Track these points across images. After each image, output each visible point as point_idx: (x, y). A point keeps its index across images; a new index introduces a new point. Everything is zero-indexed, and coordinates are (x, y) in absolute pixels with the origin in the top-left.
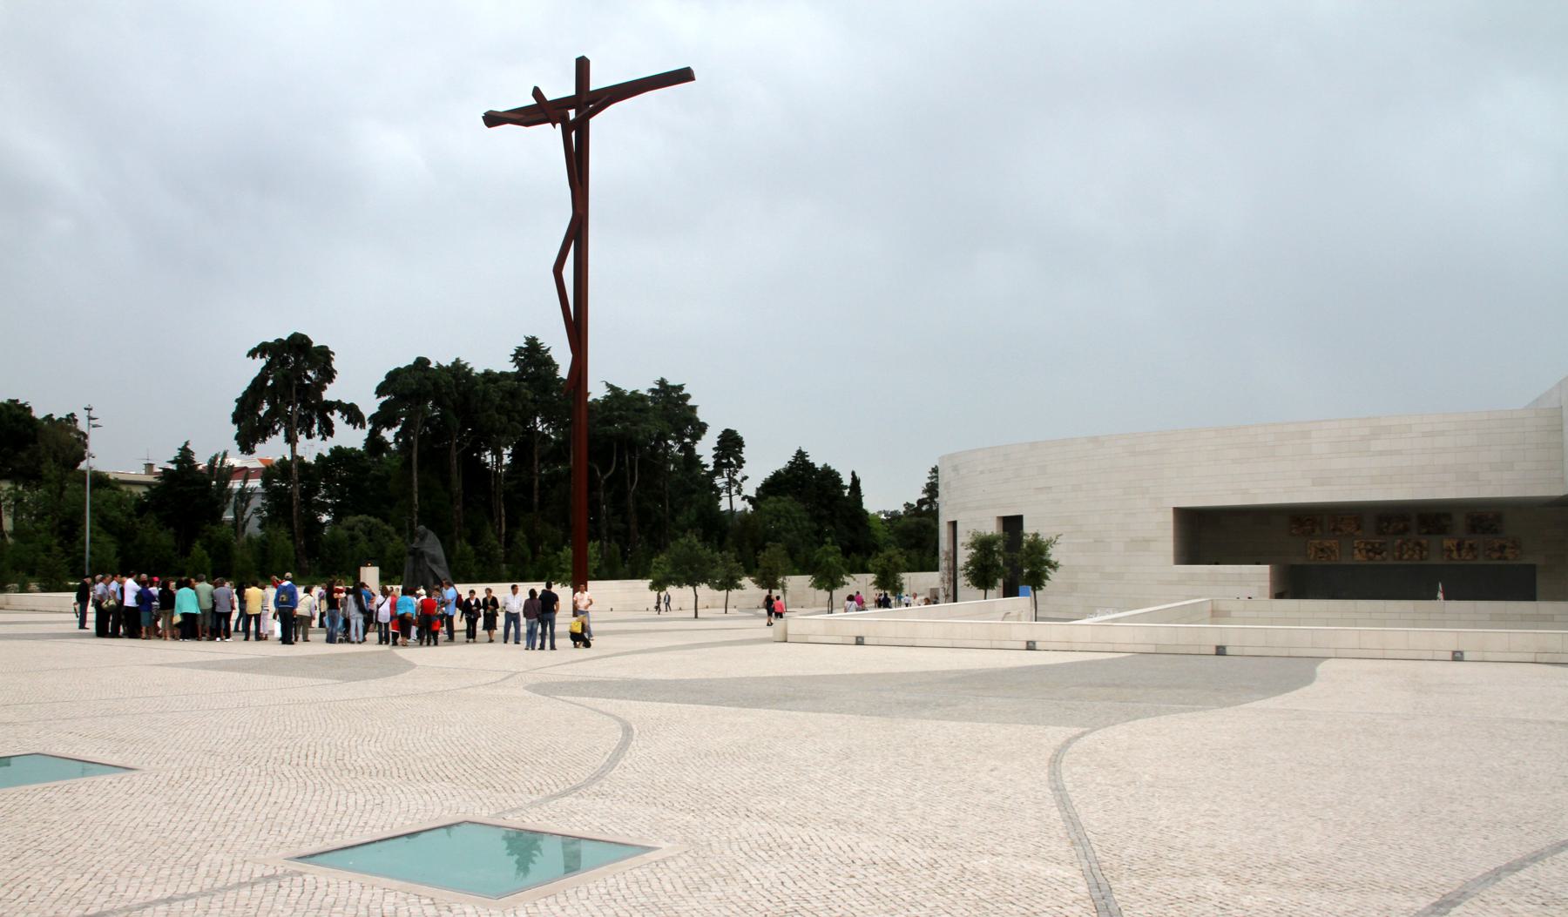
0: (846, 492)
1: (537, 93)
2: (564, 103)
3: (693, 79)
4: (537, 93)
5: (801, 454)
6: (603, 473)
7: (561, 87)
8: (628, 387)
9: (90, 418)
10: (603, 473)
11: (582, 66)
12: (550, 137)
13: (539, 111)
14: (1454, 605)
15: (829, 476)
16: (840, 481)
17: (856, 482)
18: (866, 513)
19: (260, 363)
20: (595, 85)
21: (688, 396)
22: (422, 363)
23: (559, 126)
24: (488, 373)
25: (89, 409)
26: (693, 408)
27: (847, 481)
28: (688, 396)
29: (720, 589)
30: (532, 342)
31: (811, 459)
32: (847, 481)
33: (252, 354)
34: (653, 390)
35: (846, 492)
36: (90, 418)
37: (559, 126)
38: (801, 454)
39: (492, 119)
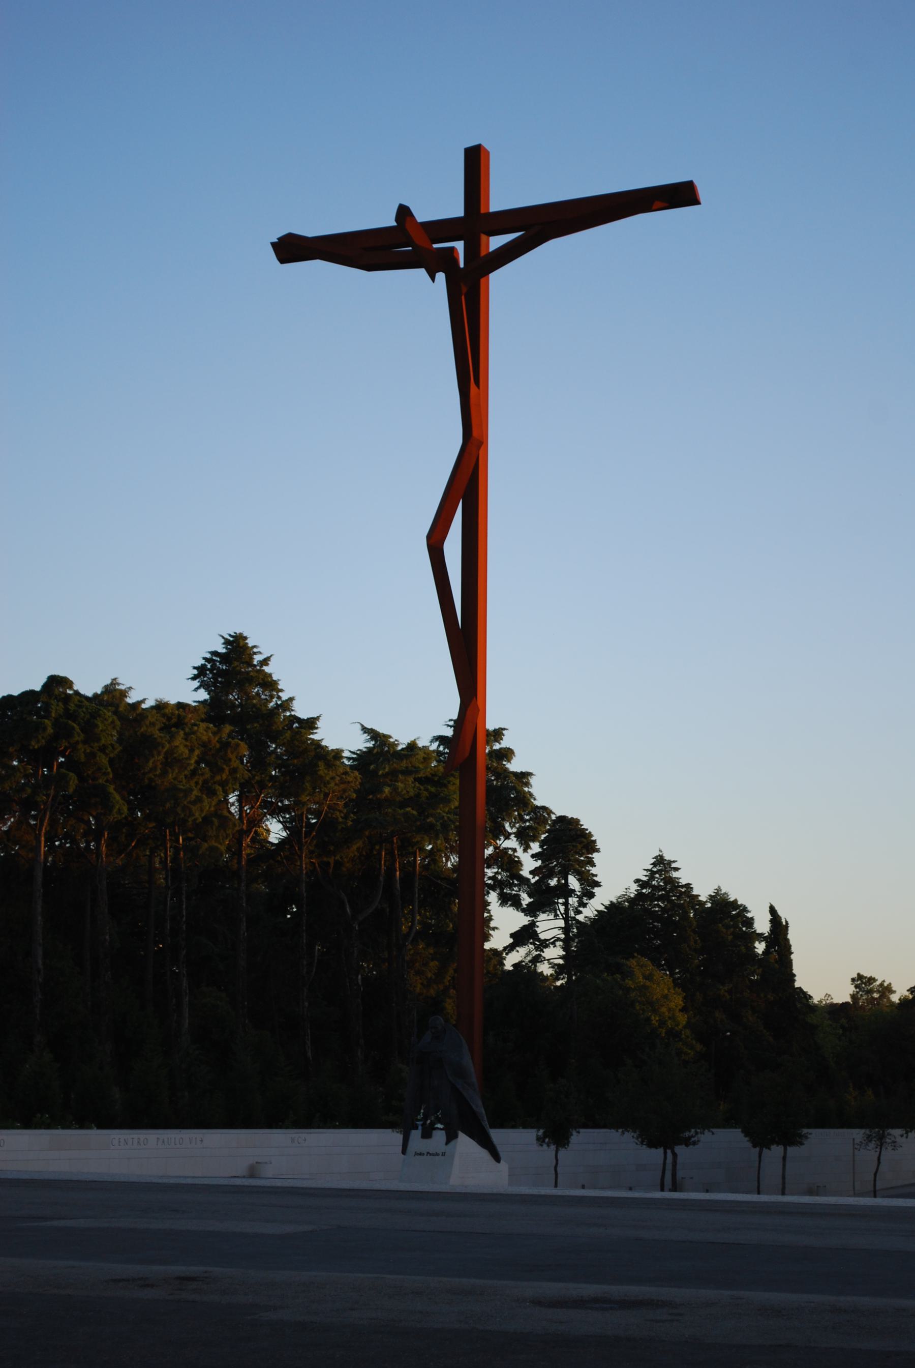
0: (760, 947)
2: (443, 229)
3: (695, 201)
5: (662, 864)
7: (443, 202)
8: (402, 737)
11: (475, 161)
12: (421, 296)
14: (100, 1131)
15: (726, 912)
16: (750, 922)
17: (779, 927)
18: (804, 996)
21: (507, 754)
22: (56, 684)
23: (441, 277)
24: (160, 707)
26: (523, 777)
27: (762, 925)
28: (507, 754)
29: (652, 1144)
30: (237, 647)
31: (683, 876)
32: (762, 925)
34: (441, 739)
35: (760, 947)
37: (441, 277)
38: (662, 864)
39: (291, 249)
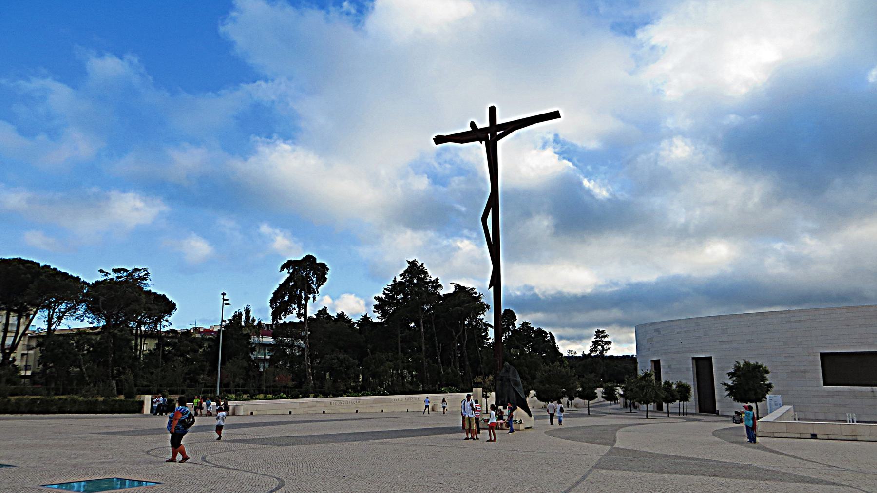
1: (473, 124)
3: (559, 117)
4: (473, 124)
6: (456, 334)
7: (483, 123)
9: (224, 300)
10: (456, 334)
11: (493, 111)
12: (479, 148)
13: (474, 134)
19: (286, 275)
20: (499, 121)
23: (484, 142)
25: (224, 294)
30: (413, 264)
33: (282, 269)
36: (224, 300)
37: (484, 142)
39: (439, 140)
